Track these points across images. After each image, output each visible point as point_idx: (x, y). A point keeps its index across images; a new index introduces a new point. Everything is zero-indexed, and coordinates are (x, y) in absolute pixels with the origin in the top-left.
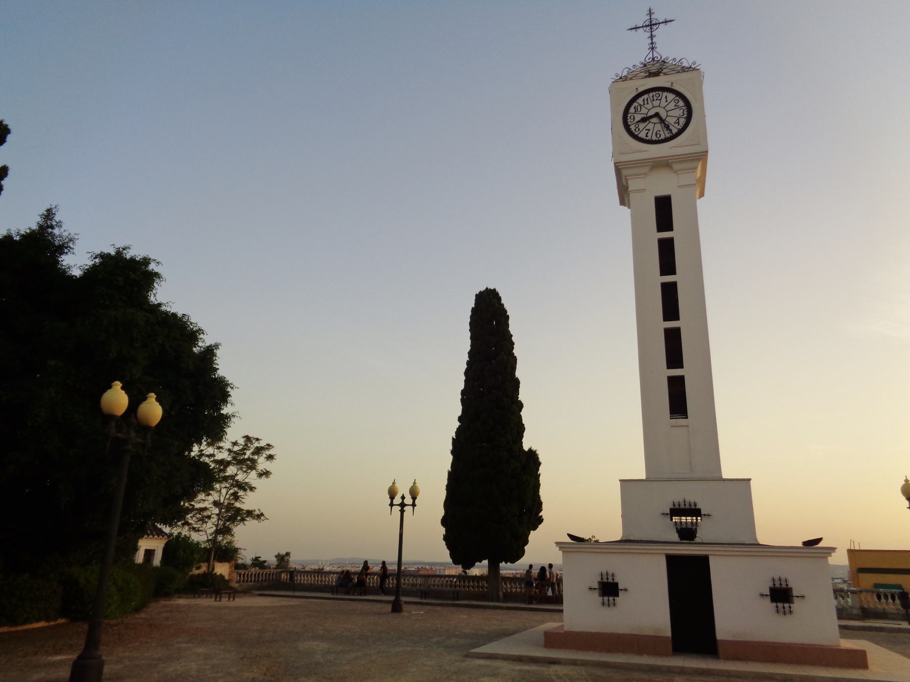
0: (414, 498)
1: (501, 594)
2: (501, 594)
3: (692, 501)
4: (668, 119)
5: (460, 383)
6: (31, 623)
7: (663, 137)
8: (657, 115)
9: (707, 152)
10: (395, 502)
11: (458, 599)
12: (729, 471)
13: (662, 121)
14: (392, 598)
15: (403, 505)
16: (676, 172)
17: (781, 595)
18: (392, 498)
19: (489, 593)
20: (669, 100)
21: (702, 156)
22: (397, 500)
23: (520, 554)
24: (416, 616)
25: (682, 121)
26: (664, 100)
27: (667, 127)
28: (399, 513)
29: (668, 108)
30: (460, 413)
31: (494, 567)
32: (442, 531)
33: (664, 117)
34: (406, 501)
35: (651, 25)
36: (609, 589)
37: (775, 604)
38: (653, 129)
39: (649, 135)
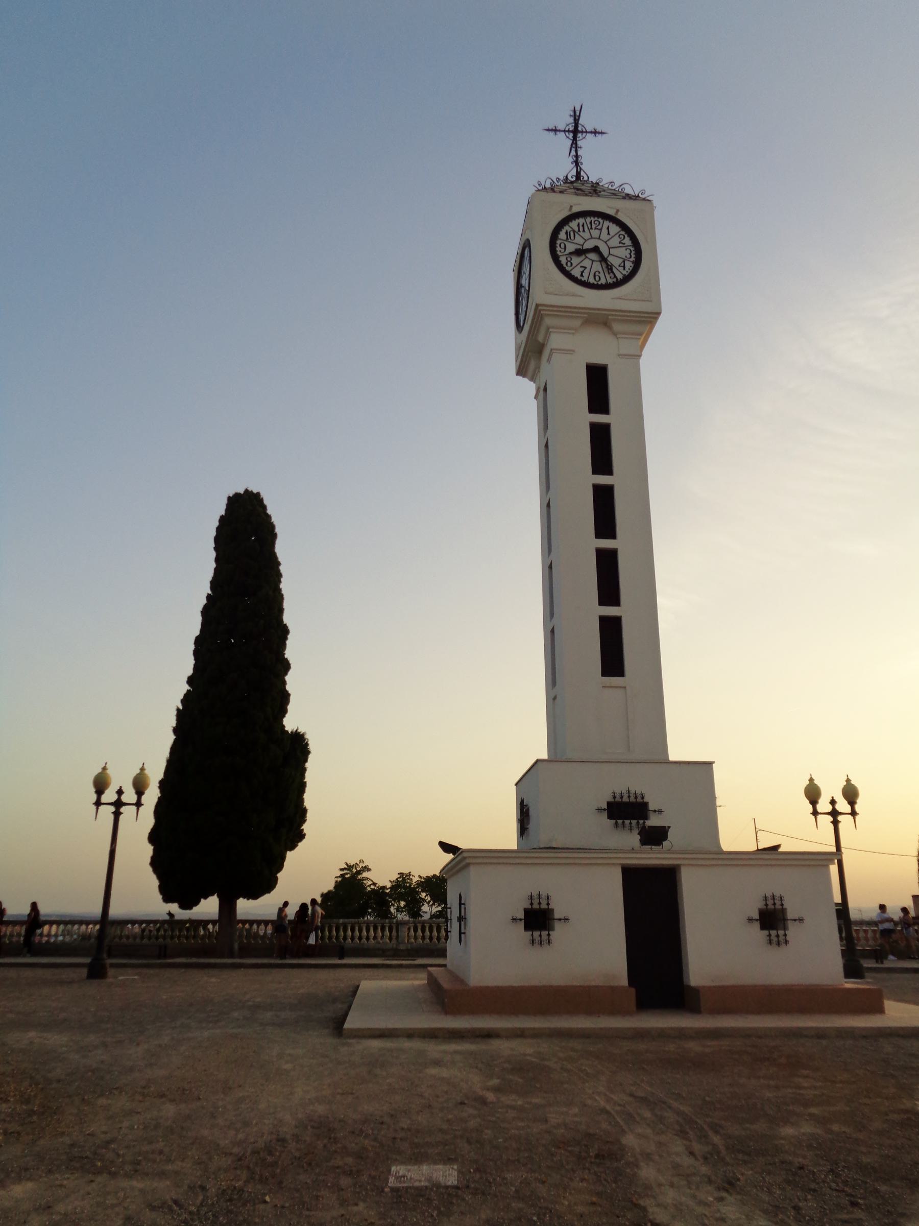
0: (852, 803)
1: (236, 946)
2: (236, 946)
3: (639, 792)
4: (611, 259)
5: (194, 626)
6: (24, 956)
7: (603, 281)
8: (596, 250)
9: (659, 314)
10: (105, 798)
11: (165, 957)
12: (677, 751)
13: (603, 259)
14: (87, 960)
15: (834, 814)
16: (615, 334)
17: (772, 919)
18: (100, 791)
19: (229, 944)
20: (612, 233)
21: (649, 318)
22: (110, 796)
23: (269, 885)
24: (128, 983)
25: (629, 265)
26: (605, 231)
27: (610, 268)
28: (112, 817)
29: (611, 243)
30: (190, 672)
31: (228, 907)
32: (149, 850)
33: (605, 254)
34: (124, 798)
35: (576, 132)
36: (538, 919)
37: (766, 932)
38: (589, 267)
39: (586, 274)
